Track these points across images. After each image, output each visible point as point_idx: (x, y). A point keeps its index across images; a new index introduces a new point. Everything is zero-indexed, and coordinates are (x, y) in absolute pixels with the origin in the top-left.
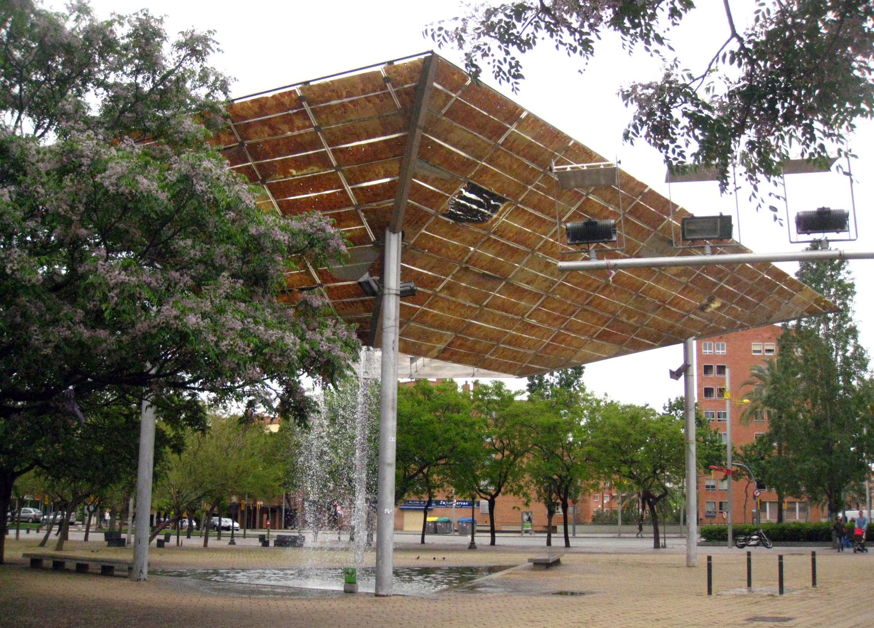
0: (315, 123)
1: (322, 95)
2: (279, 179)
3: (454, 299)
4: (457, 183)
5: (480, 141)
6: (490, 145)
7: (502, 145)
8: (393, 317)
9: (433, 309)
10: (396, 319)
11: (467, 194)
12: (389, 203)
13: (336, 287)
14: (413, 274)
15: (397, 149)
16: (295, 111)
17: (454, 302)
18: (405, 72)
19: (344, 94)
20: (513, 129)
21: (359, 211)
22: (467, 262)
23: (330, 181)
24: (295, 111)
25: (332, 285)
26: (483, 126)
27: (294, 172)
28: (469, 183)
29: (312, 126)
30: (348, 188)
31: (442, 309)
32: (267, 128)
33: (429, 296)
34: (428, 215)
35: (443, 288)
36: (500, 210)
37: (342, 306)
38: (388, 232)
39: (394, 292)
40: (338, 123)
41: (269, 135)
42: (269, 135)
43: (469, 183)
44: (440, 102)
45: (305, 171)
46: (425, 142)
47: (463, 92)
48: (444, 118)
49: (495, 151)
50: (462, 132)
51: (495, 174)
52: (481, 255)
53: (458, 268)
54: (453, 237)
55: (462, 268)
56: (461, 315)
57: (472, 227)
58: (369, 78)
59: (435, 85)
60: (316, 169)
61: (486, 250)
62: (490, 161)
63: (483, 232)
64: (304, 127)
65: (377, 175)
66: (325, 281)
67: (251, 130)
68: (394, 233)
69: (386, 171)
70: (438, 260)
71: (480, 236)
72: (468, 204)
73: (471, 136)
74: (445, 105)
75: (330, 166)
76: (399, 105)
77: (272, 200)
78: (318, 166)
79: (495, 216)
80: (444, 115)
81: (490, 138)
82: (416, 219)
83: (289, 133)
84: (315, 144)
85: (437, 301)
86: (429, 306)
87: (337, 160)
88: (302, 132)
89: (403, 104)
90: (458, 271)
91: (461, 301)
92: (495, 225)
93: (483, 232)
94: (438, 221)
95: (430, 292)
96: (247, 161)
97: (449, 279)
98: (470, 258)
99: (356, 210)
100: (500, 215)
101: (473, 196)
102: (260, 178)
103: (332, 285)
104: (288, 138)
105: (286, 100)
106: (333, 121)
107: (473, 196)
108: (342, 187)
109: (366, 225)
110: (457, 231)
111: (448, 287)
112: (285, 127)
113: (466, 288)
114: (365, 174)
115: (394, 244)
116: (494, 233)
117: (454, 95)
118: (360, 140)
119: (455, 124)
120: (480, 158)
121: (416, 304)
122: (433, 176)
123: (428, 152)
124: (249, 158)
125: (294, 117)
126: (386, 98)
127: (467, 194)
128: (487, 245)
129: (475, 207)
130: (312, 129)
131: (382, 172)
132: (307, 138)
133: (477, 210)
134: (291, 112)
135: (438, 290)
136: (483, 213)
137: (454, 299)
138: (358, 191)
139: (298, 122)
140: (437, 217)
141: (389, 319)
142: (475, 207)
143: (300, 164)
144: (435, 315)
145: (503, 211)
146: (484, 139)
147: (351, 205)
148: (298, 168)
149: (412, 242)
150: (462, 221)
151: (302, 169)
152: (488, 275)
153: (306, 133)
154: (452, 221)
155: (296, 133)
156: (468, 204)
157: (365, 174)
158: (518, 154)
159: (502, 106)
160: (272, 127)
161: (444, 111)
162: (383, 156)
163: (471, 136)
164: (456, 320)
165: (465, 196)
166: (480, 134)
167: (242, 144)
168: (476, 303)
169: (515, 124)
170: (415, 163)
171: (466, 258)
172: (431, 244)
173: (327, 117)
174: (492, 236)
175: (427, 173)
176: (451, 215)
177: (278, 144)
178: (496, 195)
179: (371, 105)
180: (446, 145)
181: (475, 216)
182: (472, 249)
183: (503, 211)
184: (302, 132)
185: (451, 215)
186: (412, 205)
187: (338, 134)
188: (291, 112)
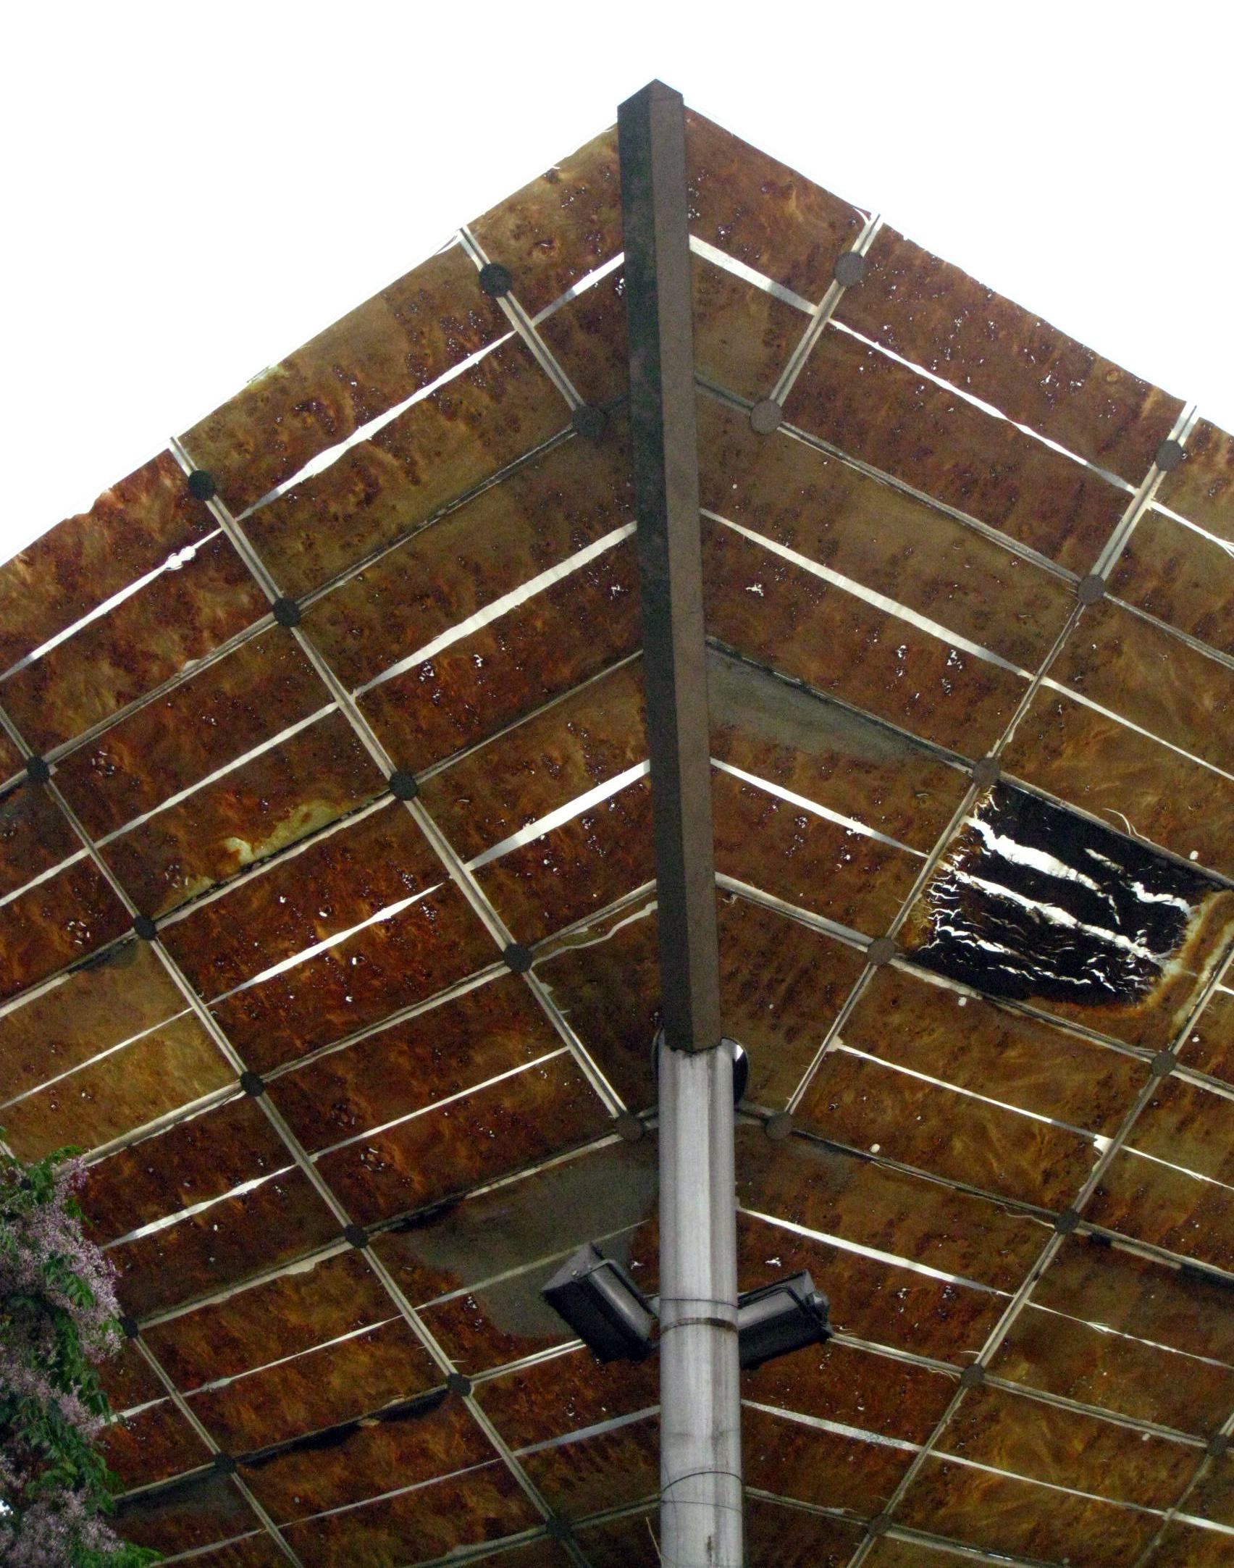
0: (273, 593)
1: (270, 442)
2: (198, 896)
3: (1072, 1405)
4: (939, 783)
5: (1001, 562)
6: (1056, 584)
7: (1119, 582)
8: (702, 1425)
9: (985, 1457)
10: (717, 1437)
11: (1006, 847)
12: (637, 906)
13: (519, 1380)
14: (839, 1267)
15: (616, 624)
16: (188, 553)
17: (1079, 1420)
18: (559, 218)
19: (348, 404)
20: (1151, 504)
21: (530, 977)
22: (1092, 1213)
23: (377, 860)
24: (188, 553)
25: (501, 1372)
26: (994, 481)
27: (243, 848)
28: (1003, 791)
29: (261, 607)
30: (463, 873)
31: (1022, 1457)
32: (106, 668)
33: (947, 1388)
34: (847, 963)
35: (1008, 1345)
36: (1193, 931)
37: (562, 1469)
38: (665, 1054)
39: (705, 1311)
40: (357, 562)
41: (122, 697)
42: (122, 697)
43: (1003, 791)
44: (751, 348)
45: (282, 834)
46: (729, 567)
47: (851, 293)
48: (791, 432)
49: (1091, 622)
50: (888, 502)
51: (1115, 743)
52: (1152, 1175)
53: (1056, 1242)
54: (993, 1073)
55: (1073, 1247)
56: (1130, 1491)
57: (1071, 1025)
58: (425, 295)
59: (700, 247)
60: (320, 810)
61: (1172, 1145)
62: (1078, 671)
63: (1144, 1056)
64: (242, 618)
65: (560, 776)
66: (472, 1360)
67: (56, 693)
68: (691, 1052)
69: (592, 745)
70: (951, 1199)
71: (1124, 1073)
72: (1029, 904)
73: (952, 531)
74: (776, 365)
75: (370, 783)
76: (573, 397)
77: (196, 1005)
78: (325, 796)
79: (1172, 968)
80: (792, 411)
81: (1051, 550)
82: (786, 984)
83: (189, 667)
84: (295, 692)
85: (992, 1418)
86: (961, 1439)
87: (391, 742)
88: (234, 644)
89: (587, 385)
90: (1059, 1261)
91: (1109, 1415)
92: (1190, 1014)
93: (1144, 1056)
94: (895, 993)
95: (950, 1370)
96: (75, 846)
97: (1022, 1299)
98: (1101, 1191)
99: (515, 976)
100: (1196, 963)
101: (1044, 862)
102: (133, 913)
103: (501, 1372)
104: (186, 688)
105: (146, 510)
106: (333, 557)
107: (1044, 862)
108: (434, 872)
109: (574, 1046)
110: (1005, 1042)
111: (1029, 1344)
112: (166, 642)
113: (1116, 1345)
114: (512, 781)
115: (697, 1106)
116: (1191, 1058)
117: (812, 309)
118: (457, 620)
119: (853, 464)
120: (1027, 653)
121: (894, 1431)
122: (814, 745)
123: (761, 616)
124: (78, 829)
125: (190, 585)
126: (514, 373)
127: (1006, 847)
128: (1169, 1120)
129: (1060, 917)
130: (266, 623)
131: (579, 756)
132: (258, 667)
133: (1077, 934)
134: (174, 562)
135: (983, 1356)
136: (1111, 949)
137: (1072, 1405)
138: (502, 876)
139: (211, 606)
140: (885, 967)
141: (684, 1436)
142: (1060, 917)
143: (260, 800)
144: (997, 1490)
145: (1206, 942)
146: (1024, 550)
147: (489, 955)
148: (256, 827)
149: (793, 1101)
150: (1018, 989)
151: (270, 829)
152: (1209, 1278)
153: (250, 647)
154: (964, 994)
155: (213, 657)
156: (1029, 904)
157: (512, 781)
158: (1203, 632)
159: (1063, 376)
160: (126, 658)
161: (780, 394)
162: (565, 671)
163: (952, 531)
164: (1117, 1515)
165: (997, 857)
166: (995, 522)
167: (37, 769)
168: (1189, 1427)
169: (1155, 476)
170: (704, 683)
171: (1086, 1191)
172: (889, 1113)
173: (310, 545)
174: (1184, 1076)
175: (785, 734)
176: (948, 958)
177: (160, 732)
178: (1148, 855)
179: (462, 427)
180: (841, 581)
181: (1073, 965)
182: (1101, 1142)
183: (1206, 942)
184: (234, 644)
185: (948, 958)
186: (747, 905)
187: (371, 612)
188: (174, 562)
